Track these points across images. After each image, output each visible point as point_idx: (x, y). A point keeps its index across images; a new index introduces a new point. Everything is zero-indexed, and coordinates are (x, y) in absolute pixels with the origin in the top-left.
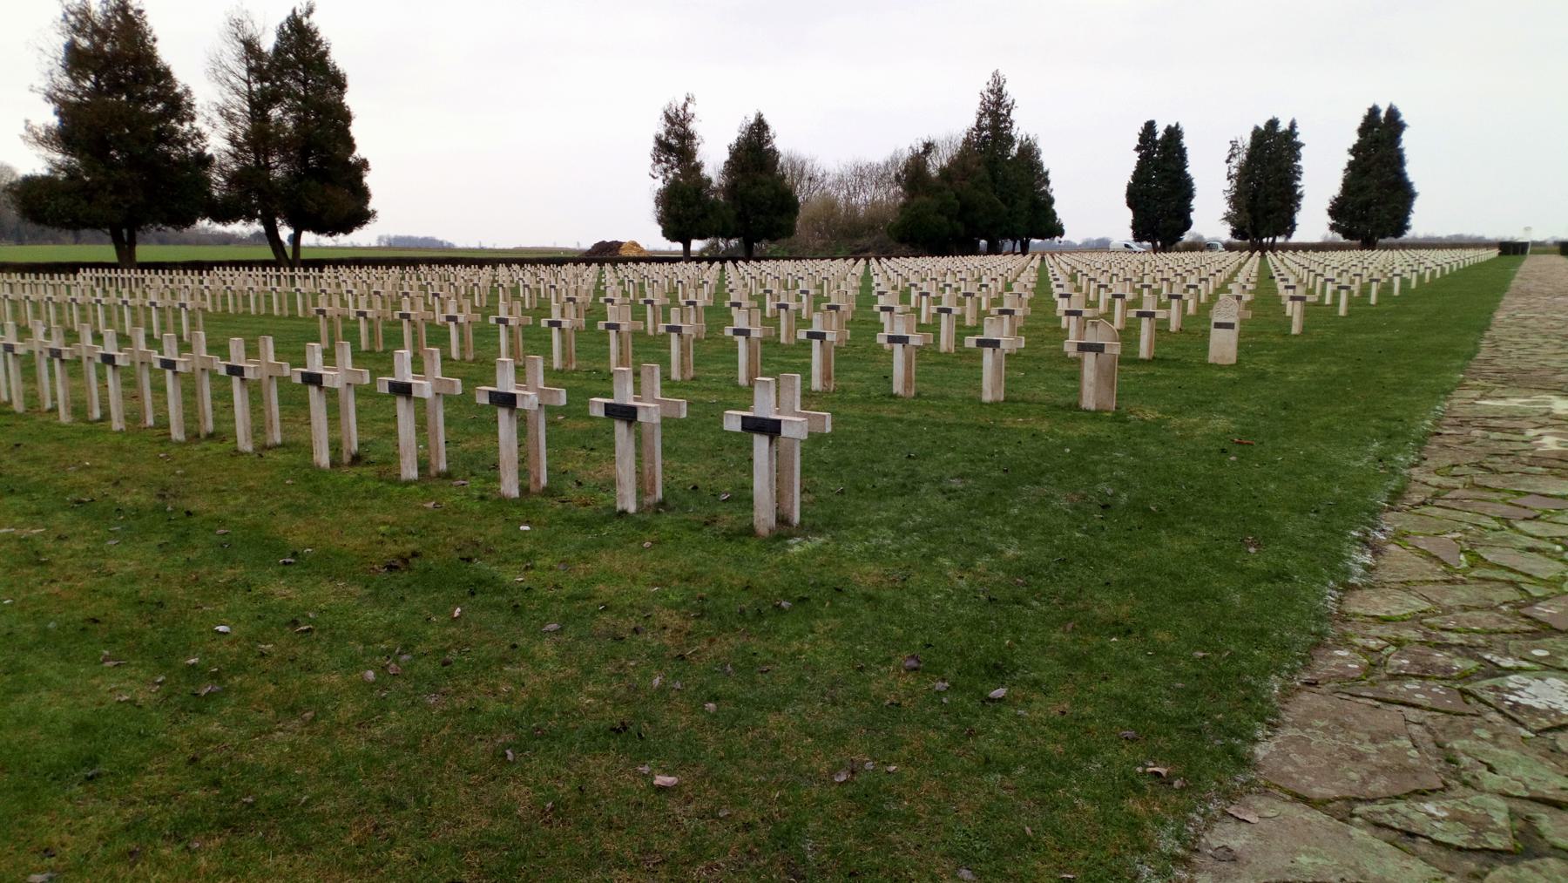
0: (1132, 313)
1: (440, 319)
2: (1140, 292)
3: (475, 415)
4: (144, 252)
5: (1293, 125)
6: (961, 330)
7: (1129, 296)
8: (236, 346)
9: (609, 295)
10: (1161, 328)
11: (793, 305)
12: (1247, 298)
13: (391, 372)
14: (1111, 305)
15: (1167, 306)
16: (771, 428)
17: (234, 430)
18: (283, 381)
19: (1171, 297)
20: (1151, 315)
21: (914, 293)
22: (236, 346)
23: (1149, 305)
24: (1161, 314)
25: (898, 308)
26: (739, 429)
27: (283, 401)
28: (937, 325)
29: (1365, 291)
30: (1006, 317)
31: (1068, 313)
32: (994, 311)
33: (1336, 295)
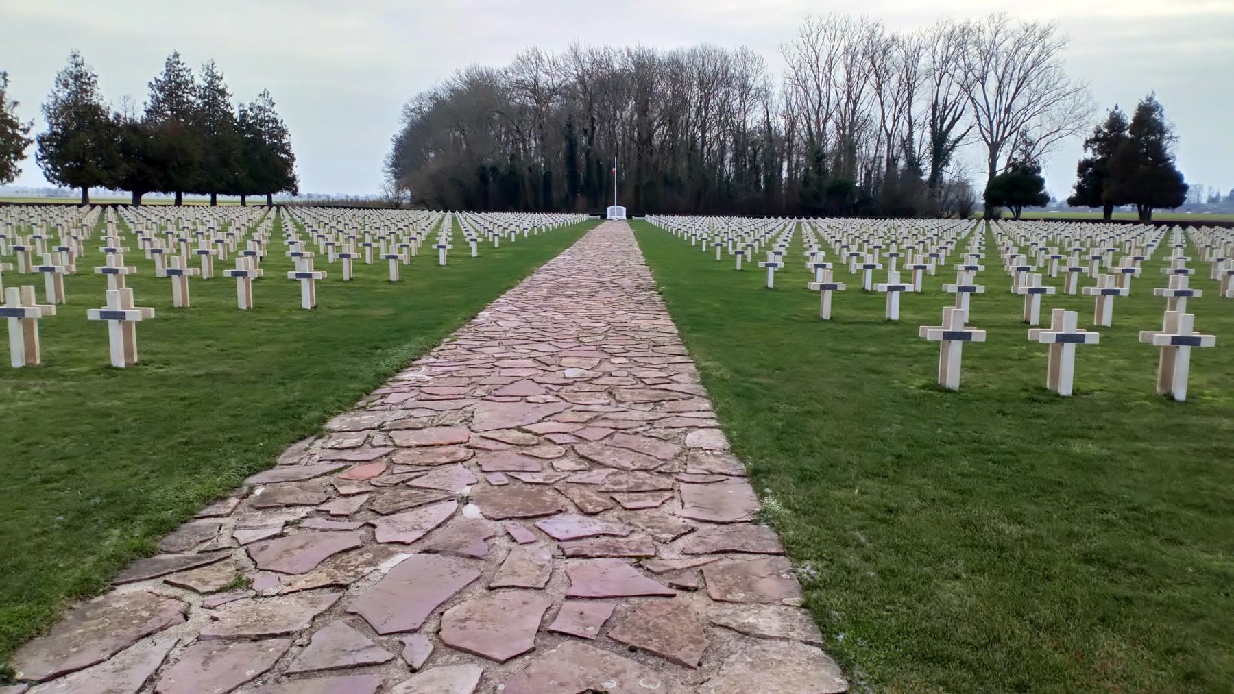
4: (1115, 215)
5: (213, 79)
6: (219, 265)
9: (111, 245)
11: (29, 247)
21: (140, 237)
30: (250, 257)
31: (153, 252)
32: (241, 253)
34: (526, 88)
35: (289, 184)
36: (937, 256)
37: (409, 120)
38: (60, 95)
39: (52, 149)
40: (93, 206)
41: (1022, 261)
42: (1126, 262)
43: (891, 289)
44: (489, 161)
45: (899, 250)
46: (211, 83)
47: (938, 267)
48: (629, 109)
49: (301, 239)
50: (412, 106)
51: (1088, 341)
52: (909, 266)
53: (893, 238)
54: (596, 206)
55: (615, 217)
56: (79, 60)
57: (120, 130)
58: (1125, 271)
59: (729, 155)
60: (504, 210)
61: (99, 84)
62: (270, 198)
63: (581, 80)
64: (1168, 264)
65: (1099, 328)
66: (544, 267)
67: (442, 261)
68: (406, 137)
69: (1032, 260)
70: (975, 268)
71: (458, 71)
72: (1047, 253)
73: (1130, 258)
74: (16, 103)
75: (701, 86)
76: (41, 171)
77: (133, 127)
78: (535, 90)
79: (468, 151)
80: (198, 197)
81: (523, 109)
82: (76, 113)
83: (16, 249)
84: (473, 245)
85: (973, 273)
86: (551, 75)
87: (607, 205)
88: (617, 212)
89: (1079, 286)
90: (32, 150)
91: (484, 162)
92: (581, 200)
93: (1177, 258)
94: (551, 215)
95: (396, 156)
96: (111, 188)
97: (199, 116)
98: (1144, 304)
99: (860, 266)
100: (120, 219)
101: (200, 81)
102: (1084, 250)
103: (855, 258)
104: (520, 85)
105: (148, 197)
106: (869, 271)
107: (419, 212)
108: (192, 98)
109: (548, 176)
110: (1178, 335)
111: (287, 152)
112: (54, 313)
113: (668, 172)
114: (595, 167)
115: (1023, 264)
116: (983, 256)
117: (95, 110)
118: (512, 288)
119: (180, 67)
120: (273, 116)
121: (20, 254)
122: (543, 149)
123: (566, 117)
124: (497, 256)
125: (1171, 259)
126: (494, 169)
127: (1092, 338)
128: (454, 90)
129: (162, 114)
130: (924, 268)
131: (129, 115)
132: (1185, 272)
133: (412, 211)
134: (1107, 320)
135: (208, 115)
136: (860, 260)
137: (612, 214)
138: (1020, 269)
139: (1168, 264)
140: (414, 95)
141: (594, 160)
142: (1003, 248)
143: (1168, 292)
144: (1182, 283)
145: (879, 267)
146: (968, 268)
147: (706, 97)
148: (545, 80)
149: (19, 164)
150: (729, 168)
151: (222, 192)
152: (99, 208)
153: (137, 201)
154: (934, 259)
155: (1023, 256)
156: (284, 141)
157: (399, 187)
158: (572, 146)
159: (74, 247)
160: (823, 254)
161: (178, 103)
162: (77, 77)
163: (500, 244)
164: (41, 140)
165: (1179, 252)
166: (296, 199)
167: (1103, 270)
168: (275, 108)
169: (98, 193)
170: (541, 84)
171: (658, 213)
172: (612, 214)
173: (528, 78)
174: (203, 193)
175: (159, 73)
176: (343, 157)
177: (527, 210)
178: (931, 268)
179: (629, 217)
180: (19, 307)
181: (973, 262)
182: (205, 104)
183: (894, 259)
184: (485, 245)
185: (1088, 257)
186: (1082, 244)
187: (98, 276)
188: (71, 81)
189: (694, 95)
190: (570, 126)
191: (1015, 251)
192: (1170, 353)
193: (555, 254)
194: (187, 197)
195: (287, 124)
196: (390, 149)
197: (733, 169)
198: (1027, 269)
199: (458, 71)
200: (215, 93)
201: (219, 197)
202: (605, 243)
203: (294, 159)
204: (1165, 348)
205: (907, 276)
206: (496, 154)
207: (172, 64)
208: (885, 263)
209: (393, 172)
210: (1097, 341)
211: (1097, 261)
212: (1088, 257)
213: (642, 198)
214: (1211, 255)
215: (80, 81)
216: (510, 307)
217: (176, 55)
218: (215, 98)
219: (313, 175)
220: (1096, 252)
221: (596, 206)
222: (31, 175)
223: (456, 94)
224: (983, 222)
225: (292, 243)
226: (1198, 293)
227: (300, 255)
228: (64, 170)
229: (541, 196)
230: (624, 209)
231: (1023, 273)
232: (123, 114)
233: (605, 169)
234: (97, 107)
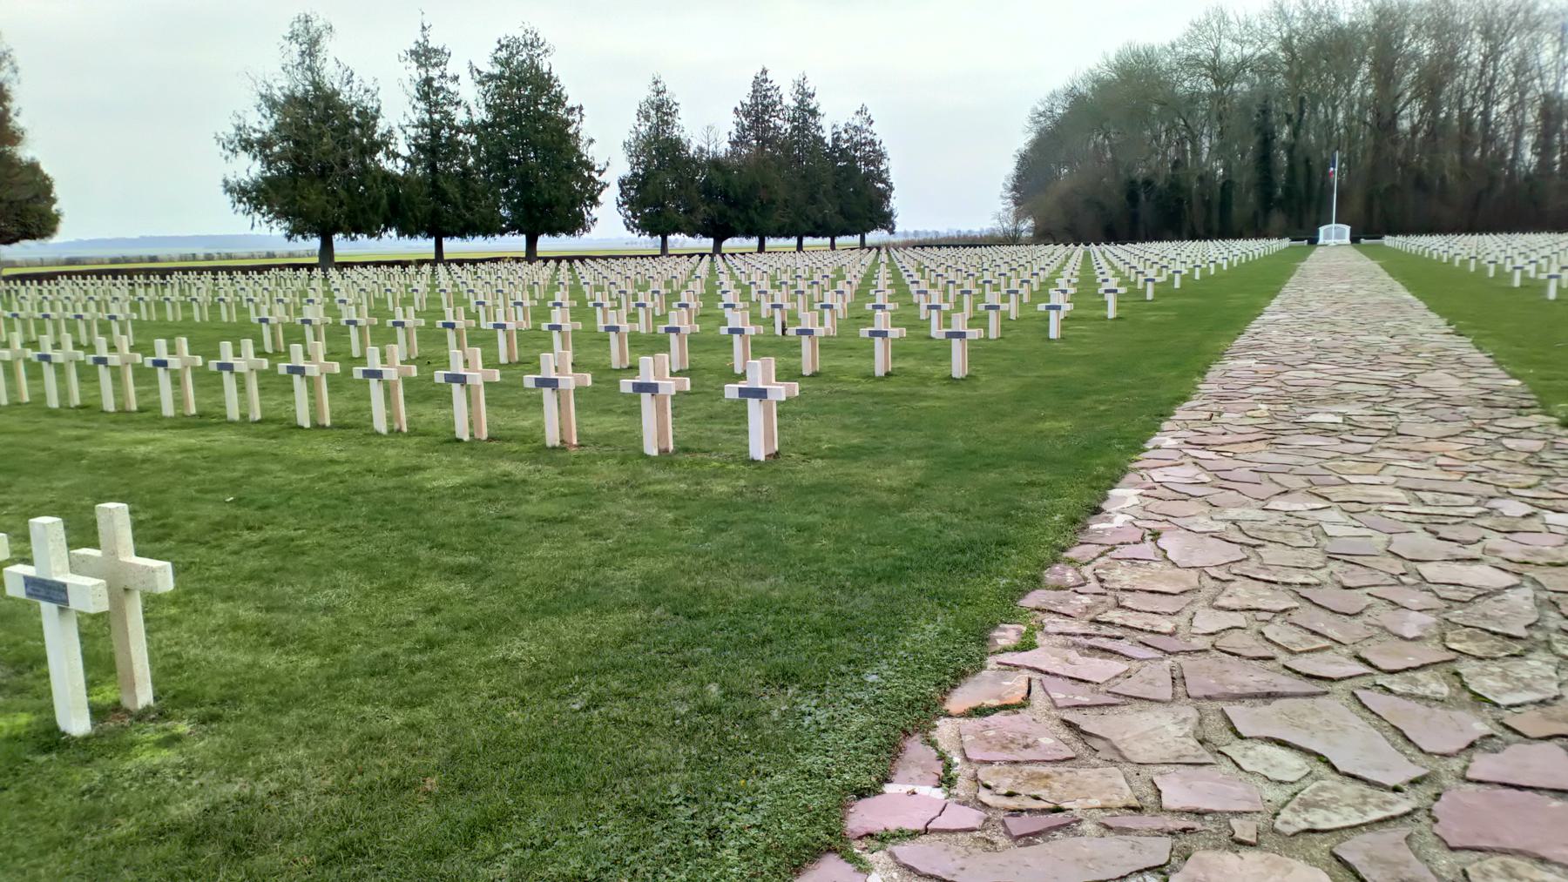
1: (486, 325)
3: (606, 394)
5: (804, 95)
8: (161, 345)
10: (1005, 318)
12: (1072, 291)
13: (153, 354)
16: (652, 388)
17: (159, 402)
18: (27, 361)
21: (754, 290)
22: (161, 345)
23: (992, 298)
25: (740, 305)
27: (80, 376)
34: (1200, 64)
35: (884, 220)
37: (1036, 128)
38: (642, 129)
39: (632, 193)
40: (546, 260)
44: (1141, 172)
46: (801, 102)
48: (1362, 84)
50: (1041, 109)
54: (1301, 226)
55: (1332, 242)
56: (660, 86)
57: (700, 166)
59: (1528, 138)
60: (1160, 239)
61: (680, 114)
62: (863, 239)
63: (1286, 45)
66: (1241, 341)
67: (1054, 333)
68: (1032, 150)
71: (1105, 56)
74: (591, 141)
75: (1487, 34)
76: (622, 218)
77: (716, 164)
78: (1218, 72)
79: (1114, 161)
80: (782, 241)
81: (1194, 98)
82: (657, 150)
83: (638, 305)
86: (1242, 43)
88: (1334, 235)
90: (610, 197)
91: (1134, 175)
92: (1277, 219)
94: (1505, 236)
95: (1018, 177)
96: (692, 235)
97: (787, 146)
100: (730, 268)
101: (789, 101)
104: (1193, 63)
105: (729, 244)
107: (1042, 247)
108: (779, 123)
109: (1227, 186)
111: (884, 181)
113: (1424, 167)
114: (1301, 170)
117: (675, 145)
118: (1185, 399)
119: (768, 85)
120: (870, 137)
121: (641, 310)
122: (1219, 151)
123: (1259, 101)
124: (1152, 317)
126: (1148, 183)
128: (1098, 80)
129: (748, 144)
131: (712, 148)
133: (1033, 247)
135: (797, 142)
140: (1044, 94)
141: (1302, 159)
147: (1492, 56)
148: (1231, 52)
149: (595, 211)
150: (1529, 156)
151: (808, 235)
152: (552, 263)
153: (717, 248)
156: (882, 167)
157: (1018, 217)
158: (1267, 141)
161: (764, 131)
162: (658, 109)
163: (1156, 293)
164: (622, 183)
166: (892, 239)
168: (873, 128)
169: (678, 241)
170: (1224, 57)
171: (1406, 232)
172: (1327, 236)
173: (1204, 51)
174: (788, 236)
175: (744, 95)
176: (953, 180)
177: (1193, 237)
179: (1355, 239)
182: (795, 128)
188: (653, 112)
189: (1474, 50)
190: (1265, 112)
193: (1254, 311)
194: (771, 242)
195: (887, 146)
196: (1009, 168)
197: (1535, 160)
199: (1105, 56)
200: (806, 113)
201: (807, 241)
202: (1338, 287)
203: (891, 189)
206: (1153, 160)
207: (760, 85)
209: (1013, 197)
213: (1377, 211)
215: (661, 110)
216: (1189, 471)
217: (764, 72)
218: (805, 121)
219: (914, 209)
221: (1301, 226)
222: (608, 224)
223: (1102, 87)
224: (317, 272)
227: (732, 306)
228: (644, 217)
229: (1216, 215)
230: (1347, 229)
232: (704, 146)
233: (1317, 171)
234: (678, 140)
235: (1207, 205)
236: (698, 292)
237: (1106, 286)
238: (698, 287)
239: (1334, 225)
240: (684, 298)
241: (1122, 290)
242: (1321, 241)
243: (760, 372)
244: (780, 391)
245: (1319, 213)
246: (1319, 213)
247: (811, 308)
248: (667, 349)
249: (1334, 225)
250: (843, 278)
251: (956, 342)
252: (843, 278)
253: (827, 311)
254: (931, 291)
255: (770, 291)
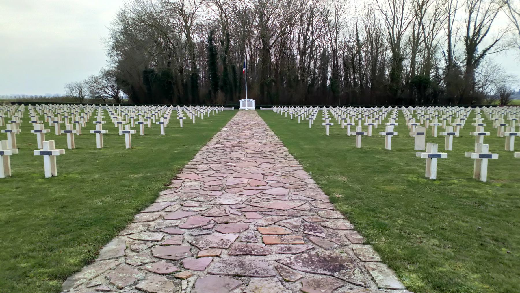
0: (137, 123)
2: (138, 116)
7: (135, 118)
10: (146, 126)
14: (130, 120)
15: (147, 120)
19: (147, 118)
20: (142, 123)
21: (46, 116)
23: (141, 120)
24: (145, 123)
26: (39, 155)
28: (139, 127)
29: (207, 113)
30: (14, 123)
33: (200, 114)
36: (378, 119)
41: (414, 121)
42: (458, 121)
43: (358, 134)
45: (362, 117)
47: (379, 125)
49: (37, 115)
51: (442, 157)
52: (366, 124)
53: (360, 112)
55: (246, 108)
58: (457, 125)
64: (475, 122)
65: (448, 152)
69: (418, 121)
70: (394, 124)
72: (424, 117)
73: (459, 119)
84: (181, 121)
85: (393, 127)
87: (240, 98)
88: (247, 104)
89: (438, 132)
92: (220, 95)
93: (479, 120)
98: (466, 140)
99: (346, 124)
102: (439, 116)
103: (343, 120)
106: (349, 126)
110: (432, 153)
112: (64, 153)
115: (414, 122)
116: (397, 119)
125: (476, 119)
127: (444, 156)
130: (372, 124)
132: (482, 125)
134: (450, 148)
136: (346, 121)
137: (244, 105)
138: (413, 125)
139: (475, 122)
142: (406, 115)
143: (476, 134)
144: (482, 130)
145: (353, 124)
146: (391, 125)
154: (377, 120)
155: (414, 119)
159: (18, 121)
160: (330, 119)
165: (479, 116)
167: (448, 125)
172: (244, 105)
178: (376, 124)
179: (257, 107)
180: (49, 150)
181: (393, 122)
183: (360, 121)
184: (188, 121)
185: (441, 119)
186: (439, 113)
187: (92, 134)
191: (411, 116)
192: (479, 161)
198: (416, 125)
204: (477, 159)
205: (365, 128)
208: (356, 122)
210: (446, 157)
211: (445, 121)
212: (441, 119)
214: (492, 117)
220: (444, 117)
221: (232, 99)
225: (32, 117)
226: (488, 134)
227: (36, 122)
230: (253, 101)
231: (414, 126)
235: (185, 86)
236: (20, 116)
237: (180, 117)
238: (20, 115)
239: (246, 99)
240: (14, 119)
241: (185, 118)
242: (241, 108)
243: (47, 146)
244: (56, 152)
245: (240, 93)
246: (240, 93)
247: (70, 123)
248: (6, 138)
249: (246, 99)
250: (84, 112)
251: (127, 135)
252: (84, 112)
253: (77, 124)
254: (118, 117)
255: (53, 117)
